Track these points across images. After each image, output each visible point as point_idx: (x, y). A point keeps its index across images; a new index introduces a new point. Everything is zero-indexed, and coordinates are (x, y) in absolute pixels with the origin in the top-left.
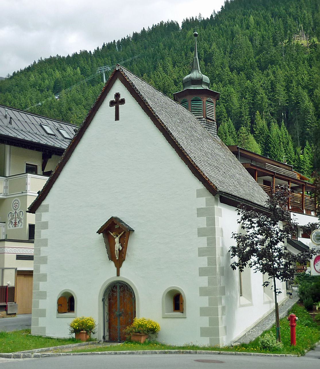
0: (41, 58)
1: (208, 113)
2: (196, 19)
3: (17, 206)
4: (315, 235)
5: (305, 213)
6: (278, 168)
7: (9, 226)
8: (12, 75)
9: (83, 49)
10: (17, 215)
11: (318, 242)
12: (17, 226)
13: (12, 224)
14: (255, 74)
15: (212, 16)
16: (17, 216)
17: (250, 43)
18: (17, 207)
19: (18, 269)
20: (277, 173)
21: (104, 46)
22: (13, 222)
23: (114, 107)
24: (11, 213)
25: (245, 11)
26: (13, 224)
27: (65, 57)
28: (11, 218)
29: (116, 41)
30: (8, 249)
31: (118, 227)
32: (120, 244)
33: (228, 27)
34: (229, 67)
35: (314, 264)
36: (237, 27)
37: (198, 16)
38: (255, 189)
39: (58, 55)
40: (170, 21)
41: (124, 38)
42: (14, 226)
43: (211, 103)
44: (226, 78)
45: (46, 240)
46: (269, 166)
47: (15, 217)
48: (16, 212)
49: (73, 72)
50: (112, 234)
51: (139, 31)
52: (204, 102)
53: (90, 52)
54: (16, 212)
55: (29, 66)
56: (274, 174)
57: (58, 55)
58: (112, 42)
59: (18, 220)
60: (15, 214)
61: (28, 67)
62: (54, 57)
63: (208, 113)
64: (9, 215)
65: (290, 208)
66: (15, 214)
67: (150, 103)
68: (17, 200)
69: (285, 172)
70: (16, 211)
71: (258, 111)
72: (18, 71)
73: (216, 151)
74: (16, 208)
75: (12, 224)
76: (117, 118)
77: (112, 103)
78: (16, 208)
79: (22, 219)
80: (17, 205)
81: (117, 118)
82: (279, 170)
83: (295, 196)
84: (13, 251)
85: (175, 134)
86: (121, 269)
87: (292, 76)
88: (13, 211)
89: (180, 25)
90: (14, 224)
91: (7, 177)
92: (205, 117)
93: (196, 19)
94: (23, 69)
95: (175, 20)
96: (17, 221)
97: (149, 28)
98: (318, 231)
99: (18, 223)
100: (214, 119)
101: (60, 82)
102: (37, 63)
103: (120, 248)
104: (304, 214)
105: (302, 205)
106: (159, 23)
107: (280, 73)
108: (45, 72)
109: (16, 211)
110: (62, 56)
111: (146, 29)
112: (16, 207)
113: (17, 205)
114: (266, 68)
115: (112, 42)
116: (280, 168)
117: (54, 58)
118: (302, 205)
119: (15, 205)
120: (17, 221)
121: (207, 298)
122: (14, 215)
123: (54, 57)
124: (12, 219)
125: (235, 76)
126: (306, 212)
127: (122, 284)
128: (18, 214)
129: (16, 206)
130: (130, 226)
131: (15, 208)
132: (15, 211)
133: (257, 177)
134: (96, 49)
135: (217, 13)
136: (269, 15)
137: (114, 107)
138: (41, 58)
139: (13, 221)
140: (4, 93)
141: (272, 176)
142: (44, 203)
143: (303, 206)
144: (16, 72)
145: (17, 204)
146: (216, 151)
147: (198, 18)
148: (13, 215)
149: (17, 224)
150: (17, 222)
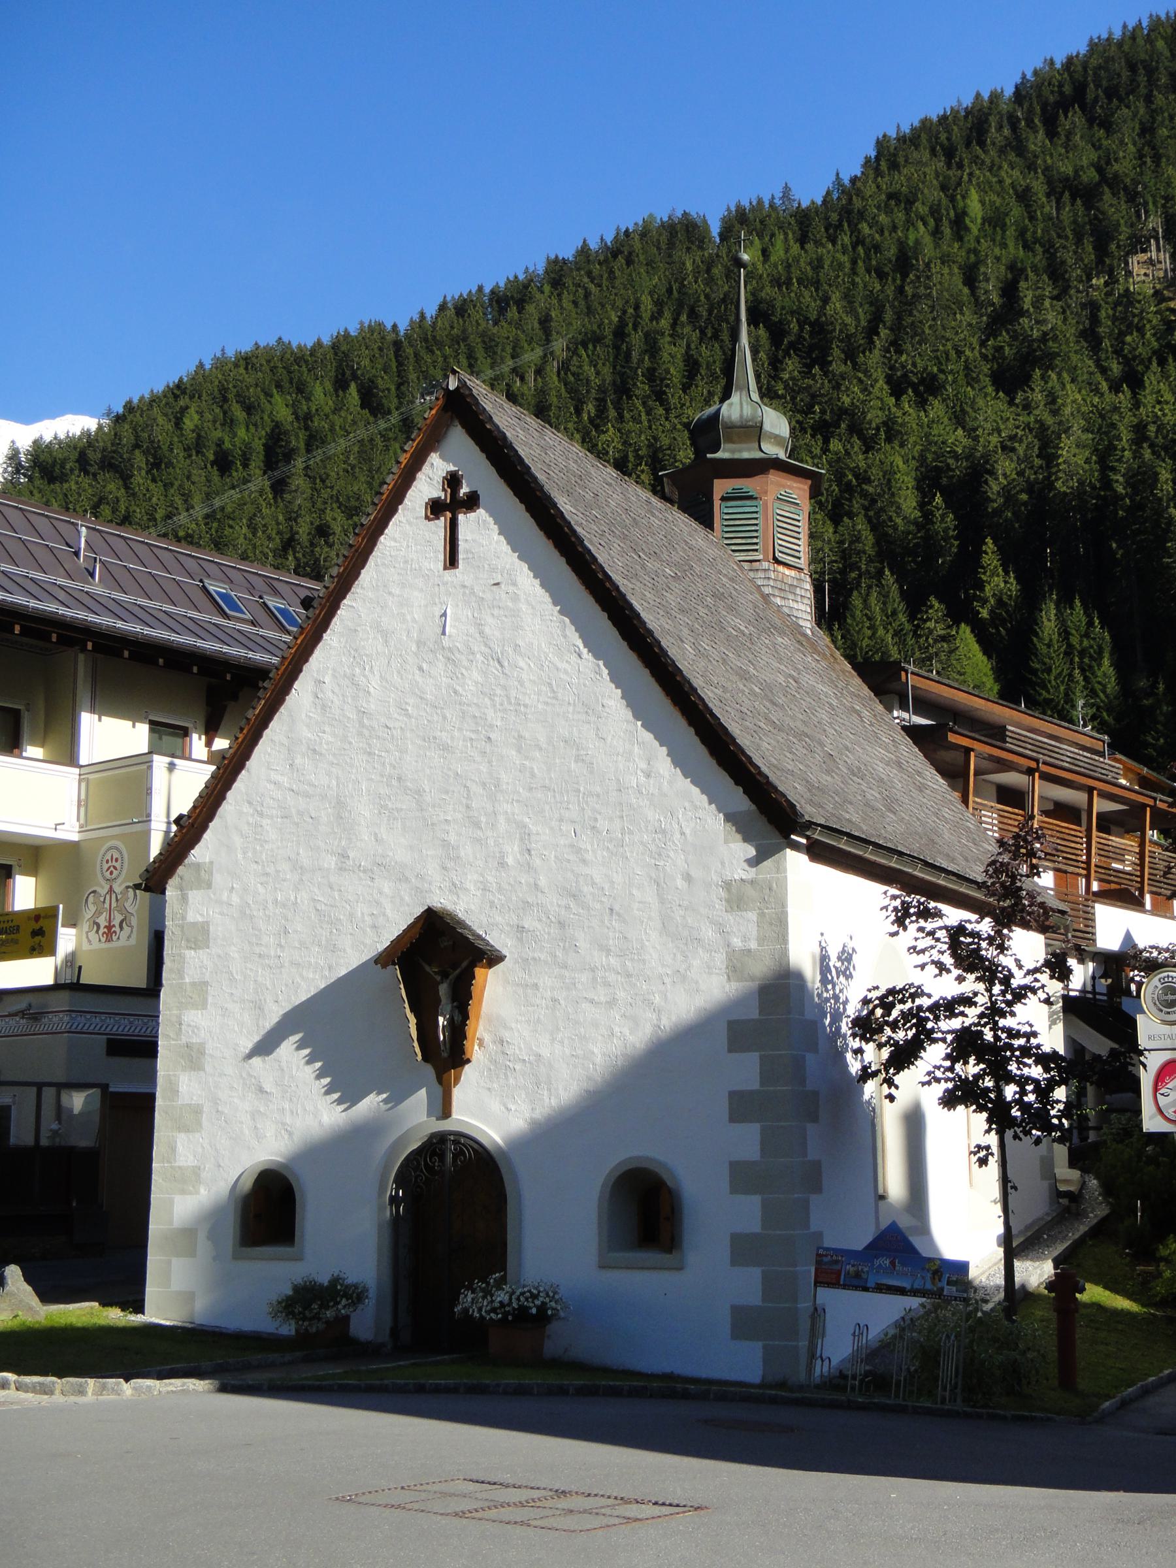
0: (223, 350)
1: (780, 542)
2: (772, 205)
3: (115, 868)
4: (1160, 986)
5: (1148, 906)
6: (1053, 743)
7: (87, 937)
8: (121, 411)
9: (369, 316)
10: (117, 900)
11: (1169, 1013)
12: (114, 938)
13: (97, 932)
14: (981, 402)
15: (828, 193)
16: (114, 904)
17: (966, 290)
18: (115, 873)
19: (111, 1089)
20: (1045, 763)
21: (443, 307)
22: (102, 927)
23: (441, 523)
24: (94, 892)
25: (950, 173)
26: (101, 932)
27: (305, 345)
28: (92, 908)
29: (487, 290)
30: (79, 1019)
31: (451, 943)
32: (455, 1004)
33: (886, 233)
34: (889, 380)
35: (1156, 1089)
36: (921, 233)
37: (779, 195)
38: (943, 816)
39: (280, 339)
40: (679, 214)
41: (516, 277)
42: (103, 939)
43: (792, 510)
44: (875, 416)
45: (202, 986)
46: (1017, 736)
47: (107, 905)
48: (111, 890)
49: (334, 398)
50: (428, 968)
51: (567, 252)
52: (766, 504)
53: (395, 326)
54: (111, 890)
55: (181, 380)
56: (1038, 764)
57: (280, 339)
58: (470, 292)
59: (118, 918)
60: (108, 897)
61: (176, 381)
62: (268, 344)
63: (780, 542)
64: (87, 900)
65: (1095, 886)
66: (108, 897)
67: (565, 505)
68: (117, 848)
69: (1078, 757)
70: (111, 887)
71: (989, 540)
72: (142, 398)
73: (808, 680)
74: (114, 876)
75: (97, 932)
76: (452, 560)
77: (435, 508)
78: (114, 876)
79: (132, 914)
80: (114, 863)
81: (452, 560)
82: (1058, 753)
83: (1114, 844)
84: (98, 1027)
85: (652, 619)
86: (457, 1093)
87: (1116, 409)
88: (103, 888)
89: (715, 229)
90: (106, 930)
91: (82, 766)
92: (771, 556)
93: (772, 205)
94: (159, 388)
95: (695, 210)
96: (116, 922)
97: (602, 239)
98: (1171, 974)
99: (117, 929)
100: (803, 562)
101: (286, 433)
102: (208, 367)
103: (456, 1018)
104: (1145, 911)
105: (1139, 879)
106: (641, 223)
107: (1073, 397)
108: (237, 402)
109: (111, 887)
110: (294, 345)
111: (594, 245)
112: (111, 873)
113: (118, 865)
114: (1024, 381)
115: (474, 291)
116: (1058, 744)
117: (268, 349)
118: (1139, 879)
119: (110, 864)
120: (116, 922)
121: (755, 1200)
122: (104, 902)
123: (268, 344)
124: (98, 913)
125: (911, 411)
126: (1153, 905)
127: (463, 1145)
128: (119, 897)
129: (112, 869)
130: (492, 942)
131: (107, 874)
132: (107, 887)
133: (975, 775)
134: (416, 317)
135: (846, 182)
136: (1039, 187)
137: (441, 523)
138: (223, 350)
139: (102, 921)
140: (95, 475)
141: (1030, 772)
142: (198, 854)
143: (1142, 883)
144: (135, 401)
145: (117, 860)
146: (808, 680)
147: (778, 202)
148: (102, 899)
149: (115, 932)
150: (114, 926)
